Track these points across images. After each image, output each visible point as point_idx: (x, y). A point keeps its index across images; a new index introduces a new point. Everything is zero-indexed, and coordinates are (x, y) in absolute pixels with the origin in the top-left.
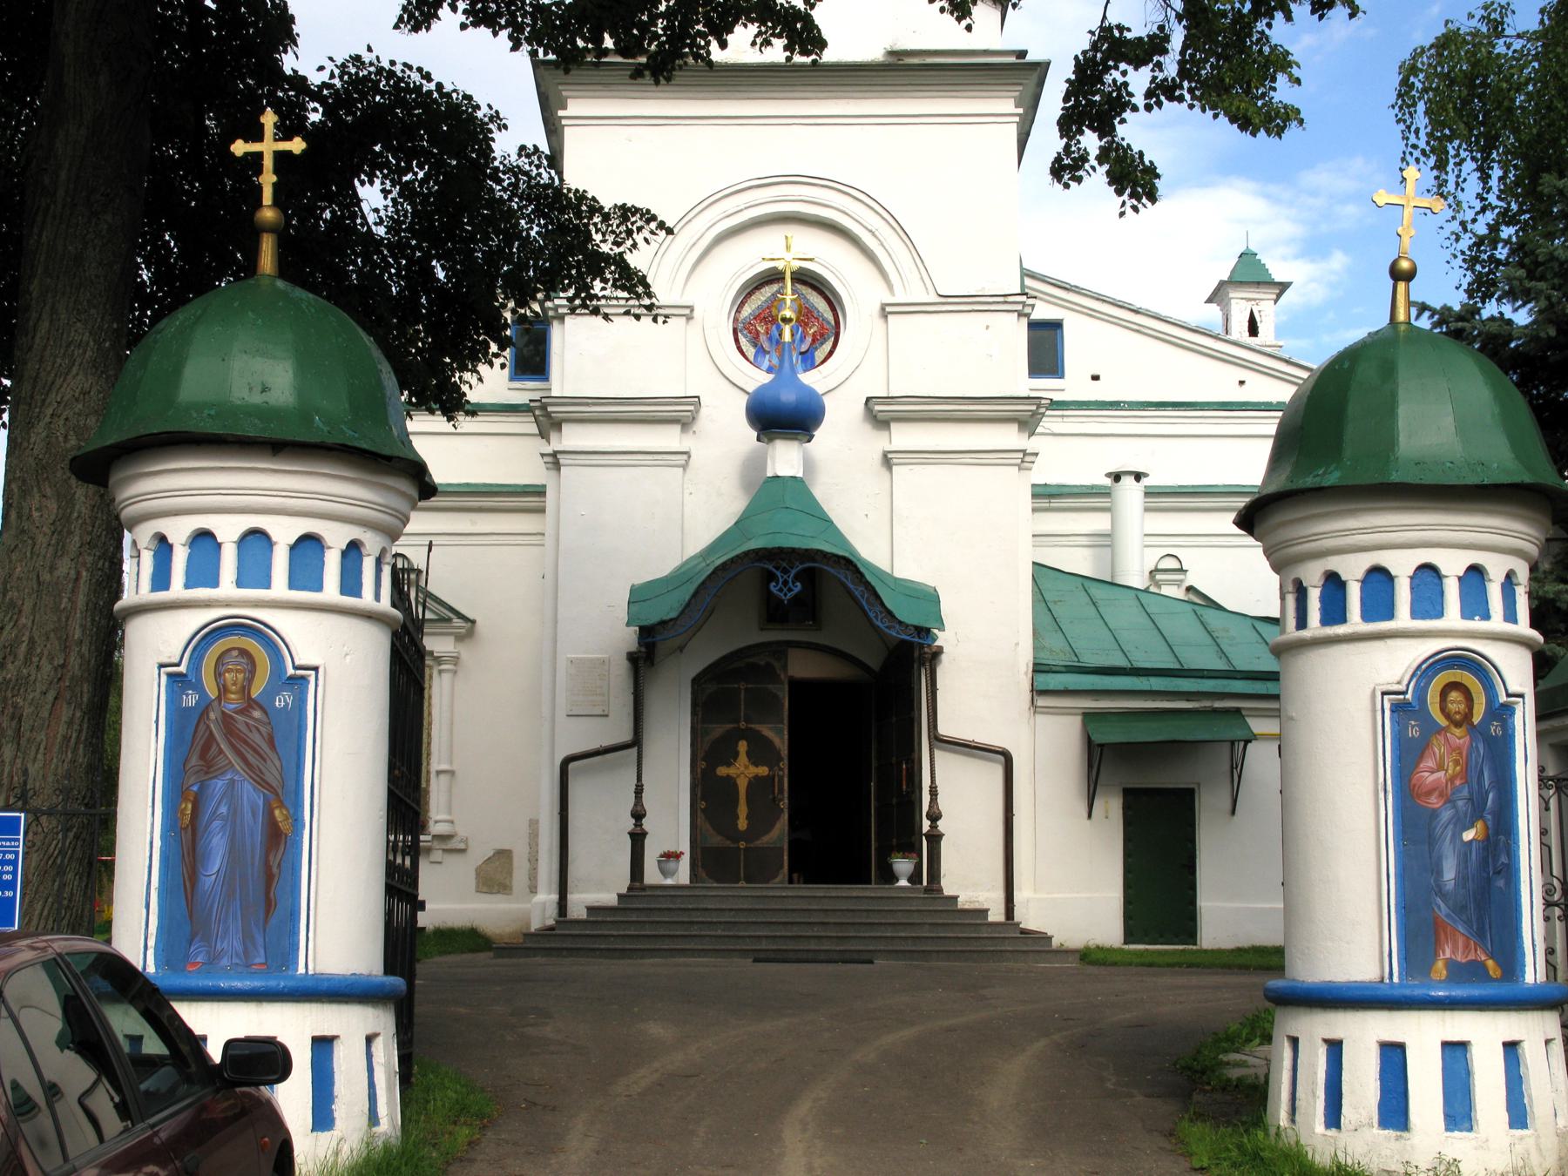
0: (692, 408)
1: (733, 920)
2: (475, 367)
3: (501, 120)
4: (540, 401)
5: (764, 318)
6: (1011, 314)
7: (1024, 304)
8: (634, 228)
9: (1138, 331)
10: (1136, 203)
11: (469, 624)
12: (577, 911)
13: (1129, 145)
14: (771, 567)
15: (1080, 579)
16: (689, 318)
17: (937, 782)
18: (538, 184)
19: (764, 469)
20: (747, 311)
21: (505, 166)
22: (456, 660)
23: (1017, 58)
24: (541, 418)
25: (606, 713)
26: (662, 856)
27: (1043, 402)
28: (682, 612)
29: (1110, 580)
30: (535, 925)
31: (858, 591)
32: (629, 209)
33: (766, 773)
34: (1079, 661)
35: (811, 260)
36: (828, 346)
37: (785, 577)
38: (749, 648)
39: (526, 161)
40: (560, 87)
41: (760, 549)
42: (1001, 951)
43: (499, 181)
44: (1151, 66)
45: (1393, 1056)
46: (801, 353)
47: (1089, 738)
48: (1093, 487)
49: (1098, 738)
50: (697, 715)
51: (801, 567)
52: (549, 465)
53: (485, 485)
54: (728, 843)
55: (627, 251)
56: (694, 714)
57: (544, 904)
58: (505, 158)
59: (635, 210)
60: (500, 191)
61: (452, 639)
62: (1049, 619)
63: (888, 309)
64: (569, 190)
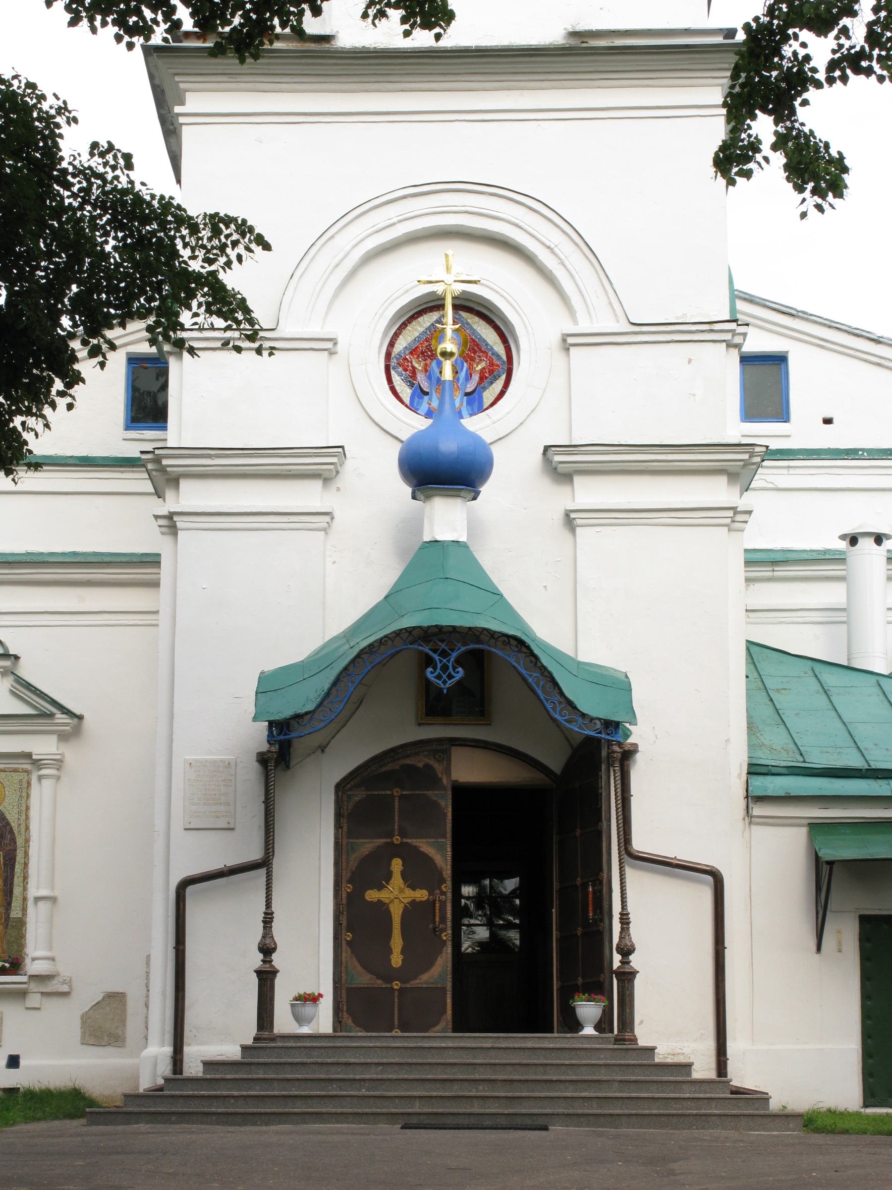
0: (334, 460)
1: (380, 1077)
2: (40, 409)
3: (70, 112)
4: (153, 452)
5: (422, 353)
6: (718, 344)
7: (732, 331)
8: (229, 243)
9: (879, 365)
10: (820, 201)
11: (76, 720)
12: (193, 1068)
13: (811, 131)
14: (426, 650)
15: (810, 663)
16: (332, 353)
17: (630, 908)
18: (115, 189)
19: (420, 532)
20: (401, 345)
21: (75, 167)
22: (59, 763)
23: (725, 38)
24: (154, 473)
25: (232, 826)
26: (296, 999)
27: (757, 449)
28: (320, 705)
29: (846, 664)
30: (145, 1084)
31: (532, 677)
32: (222, 220)
33: (425, 898)
34: (804, 762)
35: (475, 282)
36: (498, 385)
37: (445, 661)
38: (393, 750)
39: (100, 161)
40: (177, 79)
41: (414, 628)
42: (705, 1115)
43: (68, 186)
44: (835, 32)
46: (467, 394)
47: (816, 854)
48: (826, 552)
49: (828, 853)
50: (341, 828)
51: (463, 649)
52: (164, 530)
53: (95, 554)
54: (380, 983)
55: (221, 270)
56: (338, 826)
57: (156, 1058)
58: (75, 159)
59: (228, 220)
60: (69, 197)
61: (54, 738)
62: (769, 711)
63: (570, 340)
64: (153, 196)
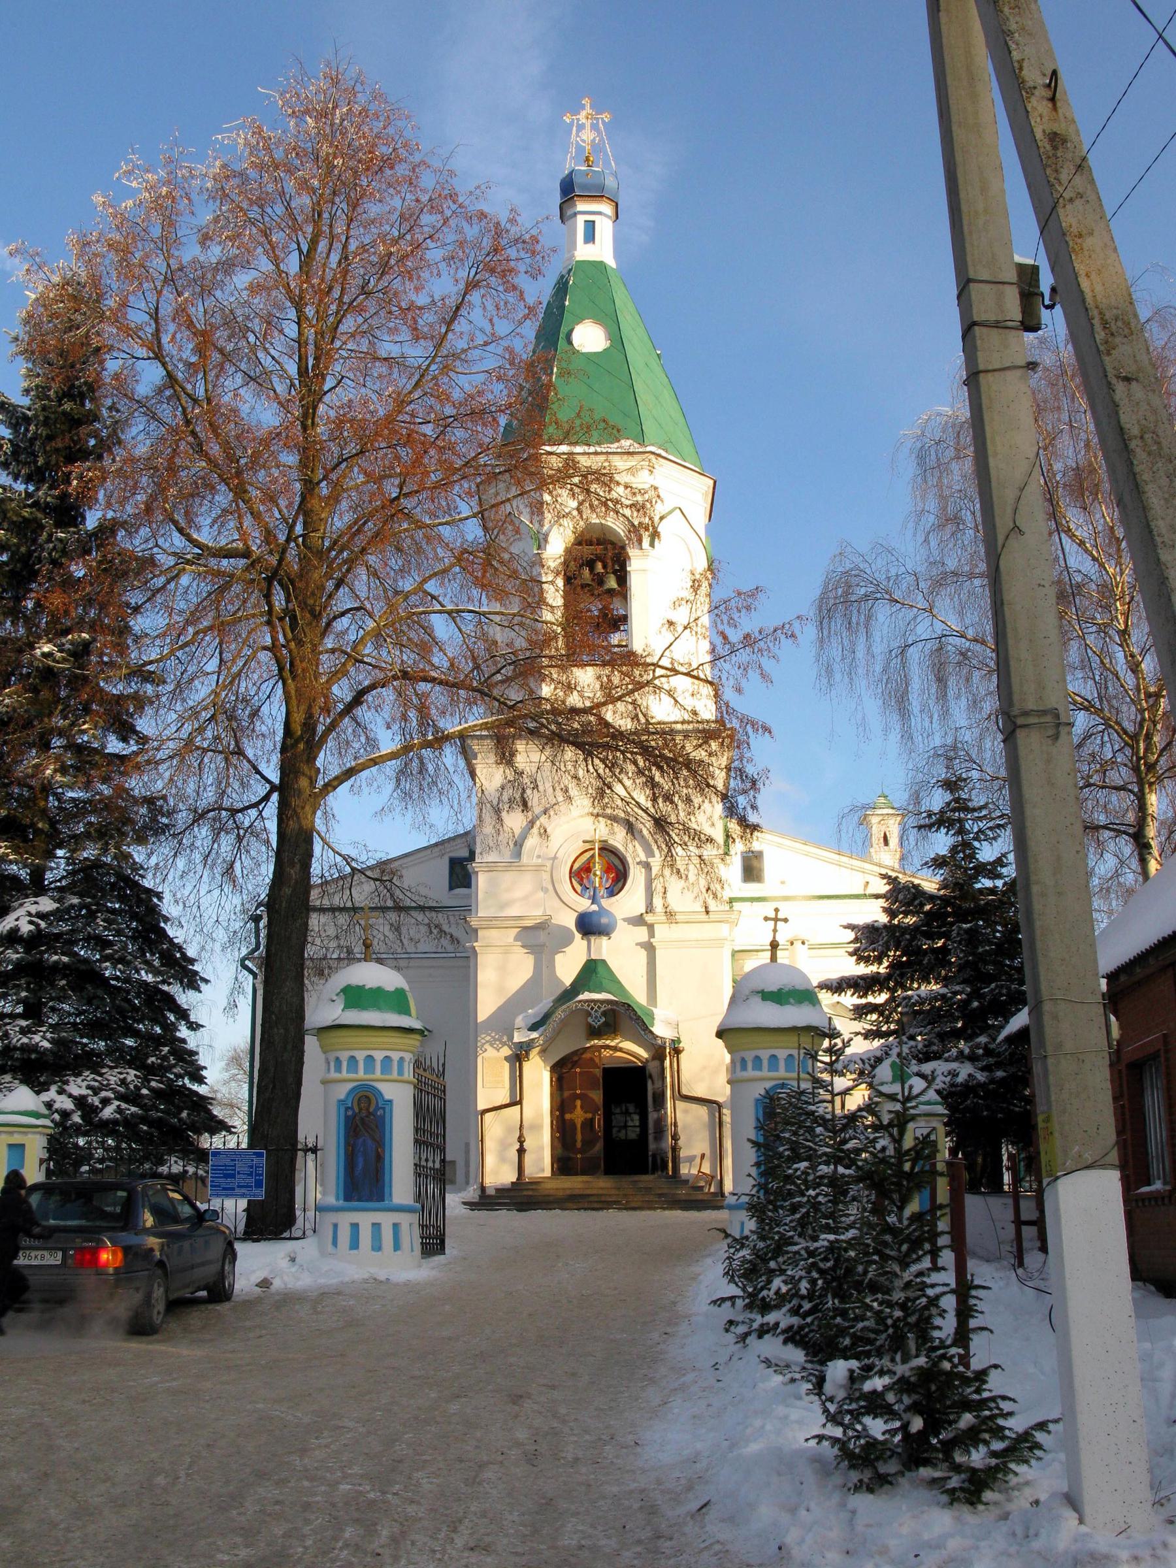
45: (355, 1227)
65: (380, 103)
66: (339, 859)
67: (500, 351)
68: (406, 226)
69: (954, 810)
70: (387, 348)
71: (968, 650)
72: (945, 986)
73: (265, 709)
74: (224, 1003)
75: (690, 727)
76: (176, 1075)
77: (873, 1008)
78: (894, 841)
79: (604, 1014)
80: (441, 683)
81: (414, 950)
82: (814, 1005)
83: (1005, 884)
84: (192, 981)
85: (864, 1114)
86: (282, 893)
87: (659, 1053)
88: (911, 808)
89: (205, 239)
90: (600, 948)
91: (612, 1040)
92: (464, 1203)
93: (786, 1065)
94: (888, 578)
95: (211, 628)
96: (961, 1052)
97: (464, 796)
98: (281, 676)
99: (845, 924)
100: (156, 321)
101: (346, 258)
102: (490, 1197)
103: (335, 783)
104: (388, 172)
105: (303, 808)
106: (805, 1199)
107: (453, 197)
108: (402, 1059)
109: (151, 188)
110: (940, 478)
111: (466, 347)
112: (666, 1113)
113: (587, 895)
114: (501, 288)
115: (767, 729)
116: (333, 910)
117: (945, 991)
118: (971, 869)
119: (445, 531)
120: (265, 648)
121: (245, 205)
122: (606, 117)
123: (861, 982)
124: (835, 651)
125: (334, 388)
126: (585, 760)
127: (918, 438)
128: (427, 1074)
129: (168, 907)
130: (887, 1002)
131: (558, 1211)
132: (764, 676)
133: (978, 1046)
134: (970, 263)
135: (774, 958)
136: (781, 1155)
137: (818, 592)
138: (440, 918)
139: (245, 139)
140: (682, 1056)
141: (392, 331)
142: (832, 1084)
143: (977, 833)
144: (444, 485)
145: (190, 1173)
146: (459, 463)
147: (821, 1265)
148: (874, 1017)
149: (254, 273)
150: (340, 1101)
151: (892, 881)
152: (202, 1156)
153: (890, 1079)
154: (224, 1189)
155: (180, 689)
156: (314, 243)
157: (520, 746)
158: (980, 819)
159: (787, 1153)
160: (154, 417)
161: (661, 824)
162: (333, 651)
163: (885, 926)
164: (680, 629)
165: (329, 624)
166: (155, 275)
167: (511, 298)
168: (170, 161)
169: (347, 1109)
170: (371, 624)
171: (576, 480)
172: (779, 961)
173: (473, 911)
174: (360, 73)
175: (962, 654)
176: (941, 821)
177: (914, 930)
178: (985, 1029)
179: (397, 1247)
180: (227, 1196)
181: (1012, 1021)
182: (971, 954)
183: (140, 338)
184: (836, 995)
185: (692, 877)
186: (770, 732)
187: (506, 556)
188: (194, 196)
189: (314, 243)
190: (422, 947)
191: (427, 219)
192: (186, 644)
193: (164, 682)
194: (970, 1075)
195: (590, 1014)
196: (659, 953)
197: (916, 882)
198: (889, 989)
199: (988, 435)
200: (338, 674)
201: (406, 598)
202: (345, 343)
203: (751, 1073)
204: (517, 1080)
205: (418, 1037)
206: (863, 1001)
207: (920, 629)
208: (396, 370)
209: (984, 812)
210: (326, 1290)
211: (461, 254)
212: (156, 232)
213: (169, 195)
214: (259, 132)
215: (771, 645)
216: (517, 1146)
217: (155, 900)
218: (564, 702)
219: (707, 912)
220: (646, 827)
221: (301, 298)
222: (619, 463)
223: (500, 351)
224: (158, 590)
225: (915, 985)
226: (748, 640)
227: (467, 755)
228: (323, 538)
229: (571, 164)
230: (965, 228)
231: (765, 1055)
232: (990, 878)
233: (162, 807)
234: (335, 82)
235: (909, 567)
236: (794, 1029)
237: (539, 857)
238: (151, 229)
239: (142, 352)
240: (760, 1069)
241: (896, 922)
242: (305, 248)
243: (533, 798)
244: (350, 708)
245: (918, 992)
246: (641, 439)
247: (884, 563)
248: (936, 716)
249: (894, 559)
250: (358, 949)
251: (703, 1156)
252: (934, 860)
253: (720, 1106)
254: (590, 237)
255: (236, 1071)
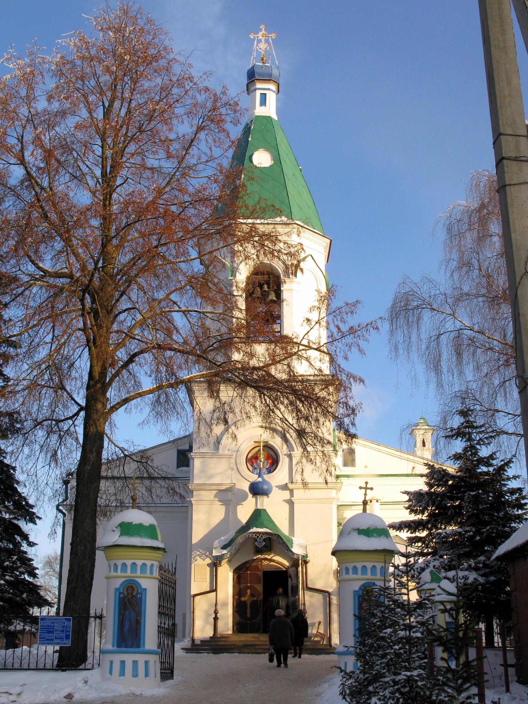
45: (123, 663)
65: (151, 25)
66: (117, 449)
67: (214, 165)
68: (164, 94)
69: (465, 427)
70: (151, 162)
71: (474, 337)
72: (460, 527)
73: (77, 363)
74: (49, 531)
75: (319, 378)
76: (20, 572)
77: (419, 539)
78: (429, 444)
79: (264, 540)
80: (180, 351)
81: (159, 502)
82: (387, 538)
83: (494, 469)
84: (32, 518)
85: (426, 602)
86: (85, 468)
87: (295, 563)
88: (441, 426)
89: (50, 98)
90: (262, 503)
91: (269, 555)
92: (183, 649)
93: (371, 572)
94: (430, 297)
95: (48, 317)
96: (470, 566)
97: (190, 415)
98: (88, 345)
99: (403, 491)
100: (22, 143)
101: (130, 112)
102: (197, 645)
103: (118, 406)
104: (154, 64)
105: (99, 420)
106: (393, 651)
107: (191, 79)
108: (152, 565)
109: (21, 68)
110: (460, 241)
111: (196, 163)
112: (299, 598)
113: (256, 472)
114: (216, 130)
115: (362, 381)
116: (113, 478)
117: (460, 530)
118: (475, 461)
119: (183, 266)
120: (80, 329)
121: (73, 80)
122: (273, 36)
123: (413, 525)
124: (399, 337)
125: (123, 184)
126: (260, 396)
127: (448, 218)
128: (166, 574)
129: (19, 476)
130: (427, 536)
131: (237, 654)
132: (361, 350)
133: (479, 562)
134: (501, 125)
135: (365, 510)
136: (375, 625)
137: (391, 303)
138: (175, 484)
139: (75, 43)
140: (309, 565)
141: (154, 153)
142: (407, 584)
143: (479, 441)
144: (181, 240)
145: (27, 630)
146: (191, 228)
147: (402, 690)
148: (420, 544)
149: (77, 119)
150: (116, 589)
151: (431, 467)
152: (34, 620)
153: (429, 580)
154: (47, 640)
155: (30, 353)
156: (112, 102)
157: (222, 387)
158: (480, 432)
159: (378, 623)
160: (18, 196)
161: (301, 433)
162: (117, 332)
163: (427, 493)
164: (313, 323)
165: (116, 316)
166: (23, 117)
167: (222, 136)
168: (32, 53)
169: (120, 593)
170: (139, 317)
171: (256, 239)
172: (368, 512)
173: (191, 480)
174: (140, 8)
175: (470, 339)
176: (459, 433)
177: (443, 495)
178: (483, 552)
179: (147, 675)
180: (49, 644)
181: (500, 548)
182: (475, 510)
183: (12, 152)
184: (398, 532)
185: (318, 464)
186: (363, 382)
187: (216, 280)
188: (45, 74)
189: (112, 102)
190: (163, 501)
191: (175, 91)
192: (35, 326)
193: (21, 347)
194: (475, 579)
195: (256, 540)
196: (296, 506)
197: (444, 468)
198: (428, 529)
199: (511, 221)
200: (119, 345)
201: (160, 303)
202: (129, 159)
203: (351, 576)
204: (214, 577)
205: (161, 552)
206: (413, 535)
207: (447, 325)
208: (156, 175)
209: (483, 429)
210: (106, 700)
211: (194, 111)
212: (23, 93)
213: (32, 72)
214: (82, 39)
215: (365, 333)
216: (214, 616)
217: (12, 471)
218: (248, 363)
219: (326, 483)
220: (292, 436)
221: (104, 133)
222: (281, 229)
223: (214, 165)
224: (19, 295)
225: (443, 527)
226: (352, 331)
227: (190, 392)
228: (113, 268)
229: (253, 61)
230: (498, 105)
231: (359, 565)
232: (486, 466)
233: (17, 418)
234: (126, 13)
235: (442, 291)
236: (376, 551)
237: (229, 450)
238: (21, 91)
239: (13, 161)
240: (357, 574)
241: (433, 490)
242: (107, 104)
243: (230, 417)
244: (126, 365)
245: (445, 531)
246: (290, 216)
247: (428, 288)
248: (455, 374)
249: (433, 286)
250: (128, 501)
251: (320, 623)
252: (454, 456)
253: (329, 594)
254: (263, 102)
255: (49, 570)
